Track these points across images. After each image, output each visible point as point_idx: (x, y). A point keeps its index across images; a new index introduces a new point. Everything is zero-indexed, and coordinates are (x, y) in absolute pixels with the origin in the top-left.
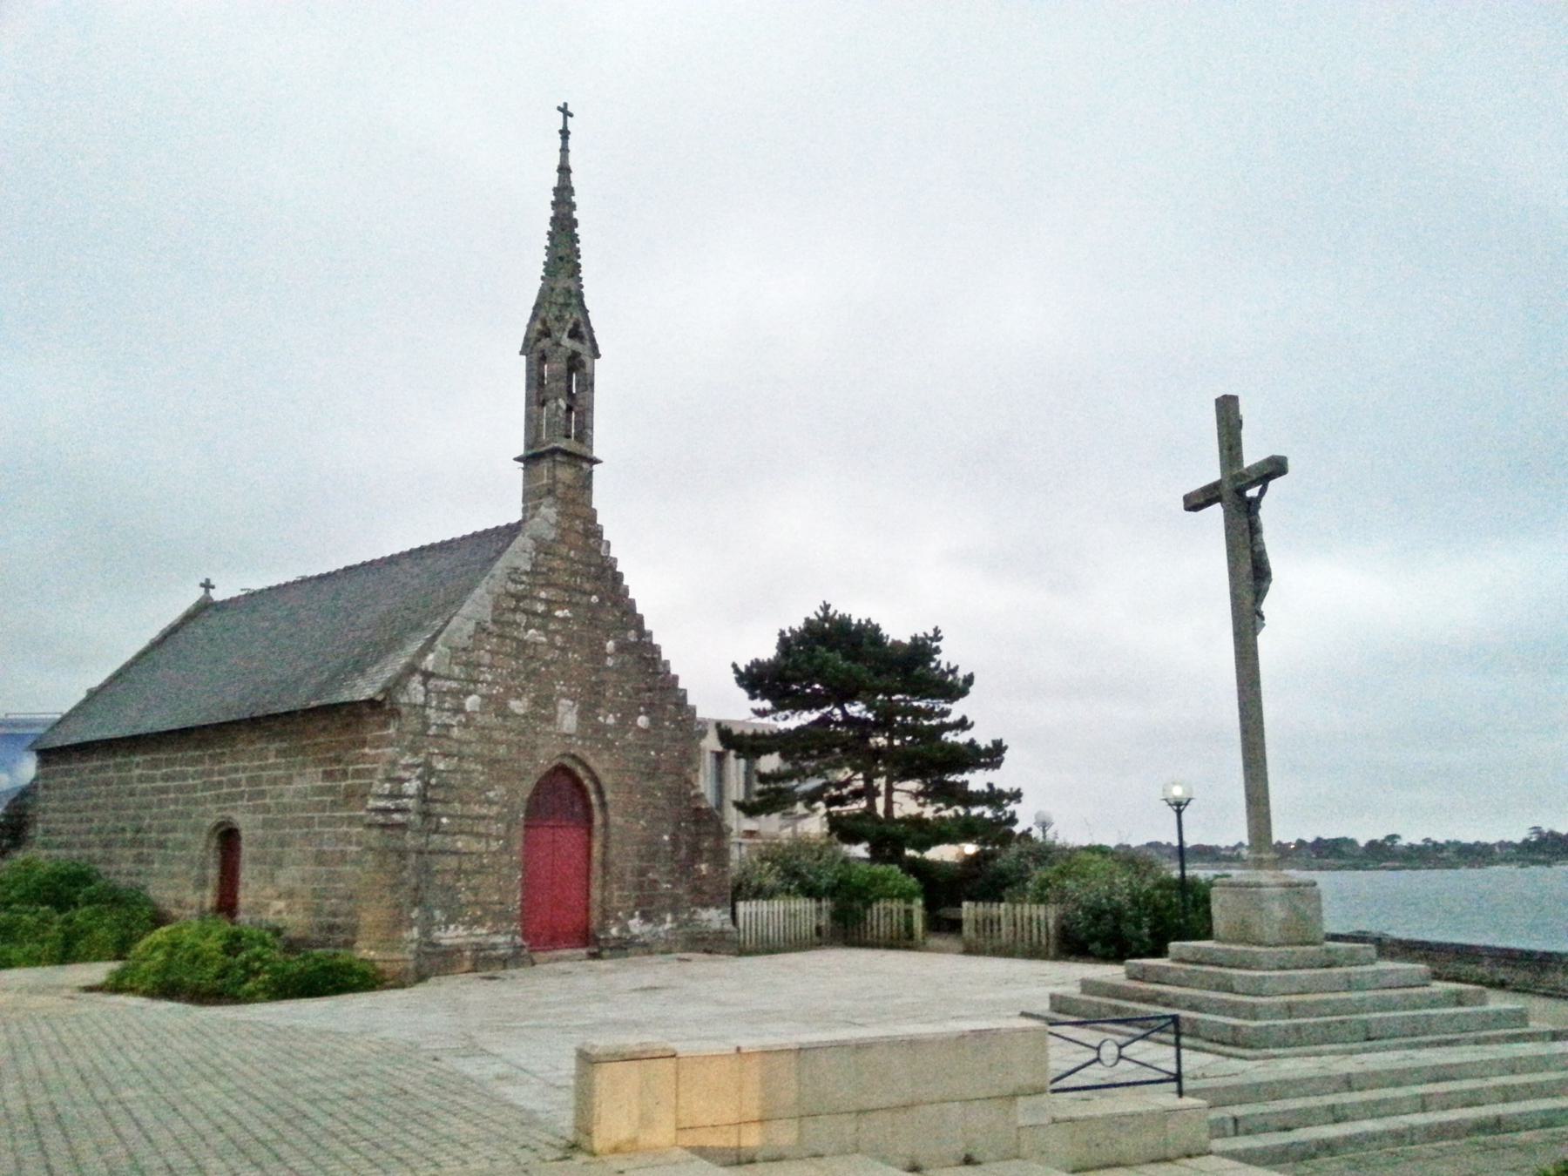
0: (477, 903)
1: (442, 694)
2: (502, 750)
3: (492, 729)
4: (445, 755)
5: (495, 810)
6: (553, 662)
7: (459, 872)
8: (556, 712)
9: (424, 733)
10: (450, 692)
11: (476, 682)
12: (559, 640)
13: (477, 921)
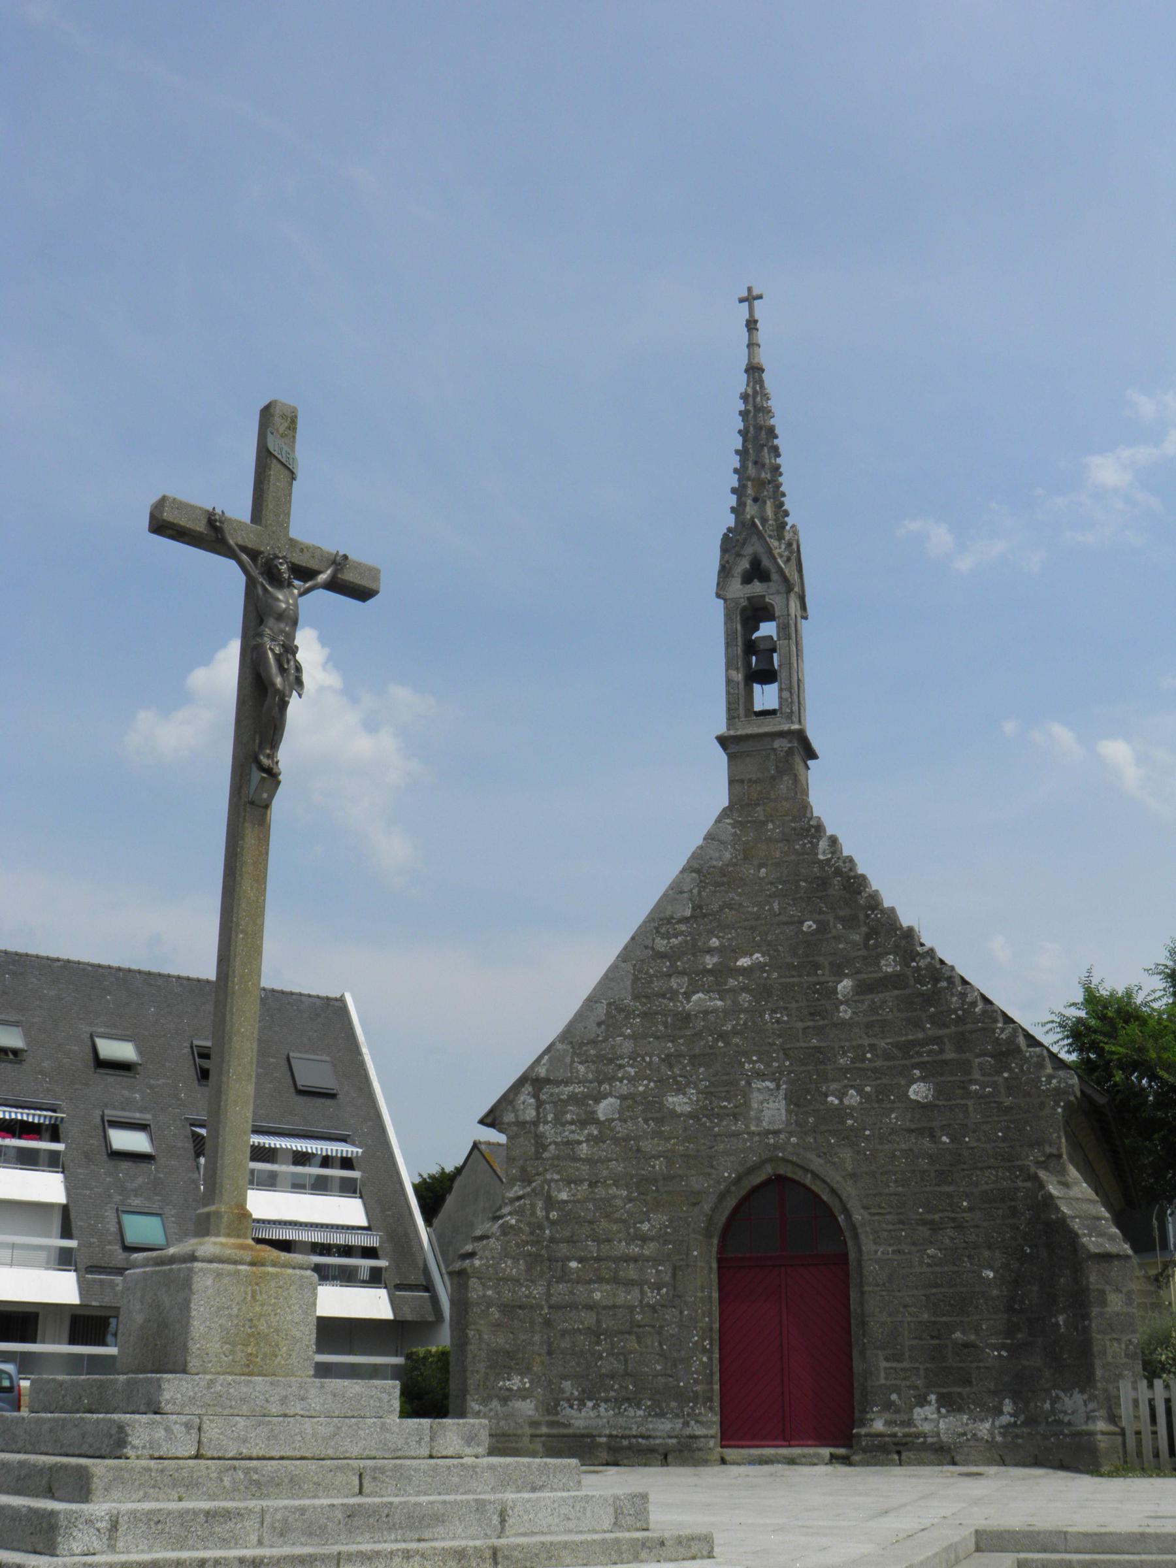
0: (627, 1374)
1: (560, 1105)
2: (658, 1165)
3: (637, 1139)
4: (569, 1182)
5: (650, 1249)
6: (735, 1032)
7: (595, 1333)
8: (747, 1104)
9: (538, 1157)
10: (574, 1099)
11: (611, 1079)
12: (745, 998)
13: (633, 1401)
